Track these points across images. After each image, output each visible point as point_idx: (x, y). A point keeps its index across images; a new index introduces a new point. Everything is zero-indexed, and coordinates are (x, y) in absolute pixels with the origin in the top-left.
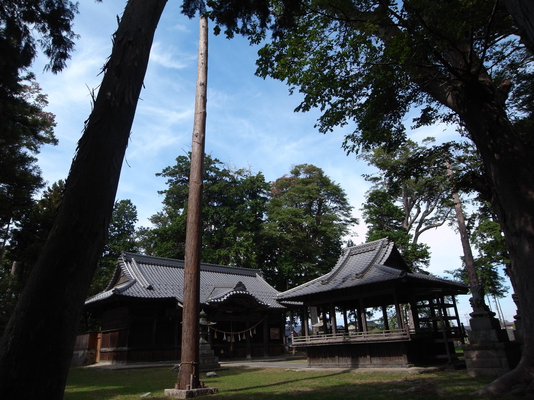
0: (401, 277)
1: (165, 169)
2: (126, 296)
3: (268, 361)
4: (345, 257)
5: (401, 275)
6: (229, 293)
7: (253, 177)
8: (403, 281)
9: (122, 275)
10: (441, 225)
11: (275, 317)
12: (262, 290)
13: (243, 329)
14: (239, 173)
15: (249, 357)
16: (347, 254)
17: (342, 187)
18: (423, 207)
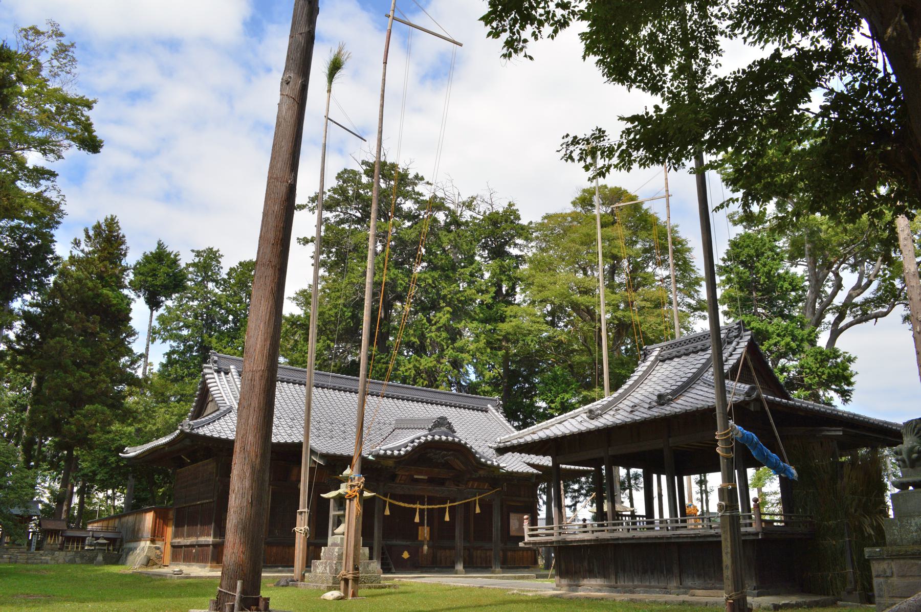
0: (747, 399)
1: (313, 195)
2: (204, 437)
3: (515, 578)
4: (648, 363)
5: (748, 394)
6: (419, 438)
7: (497, 213)
8: (752, 409)
9: (210, 399)
10: (885, 314)
11: (518, 493)
12: (484, 431)
13: (436, 508)
14: (469, 205)
15: (460, 567)
16: (652, 358)
17: (624, 187)
18: (849, 278)
